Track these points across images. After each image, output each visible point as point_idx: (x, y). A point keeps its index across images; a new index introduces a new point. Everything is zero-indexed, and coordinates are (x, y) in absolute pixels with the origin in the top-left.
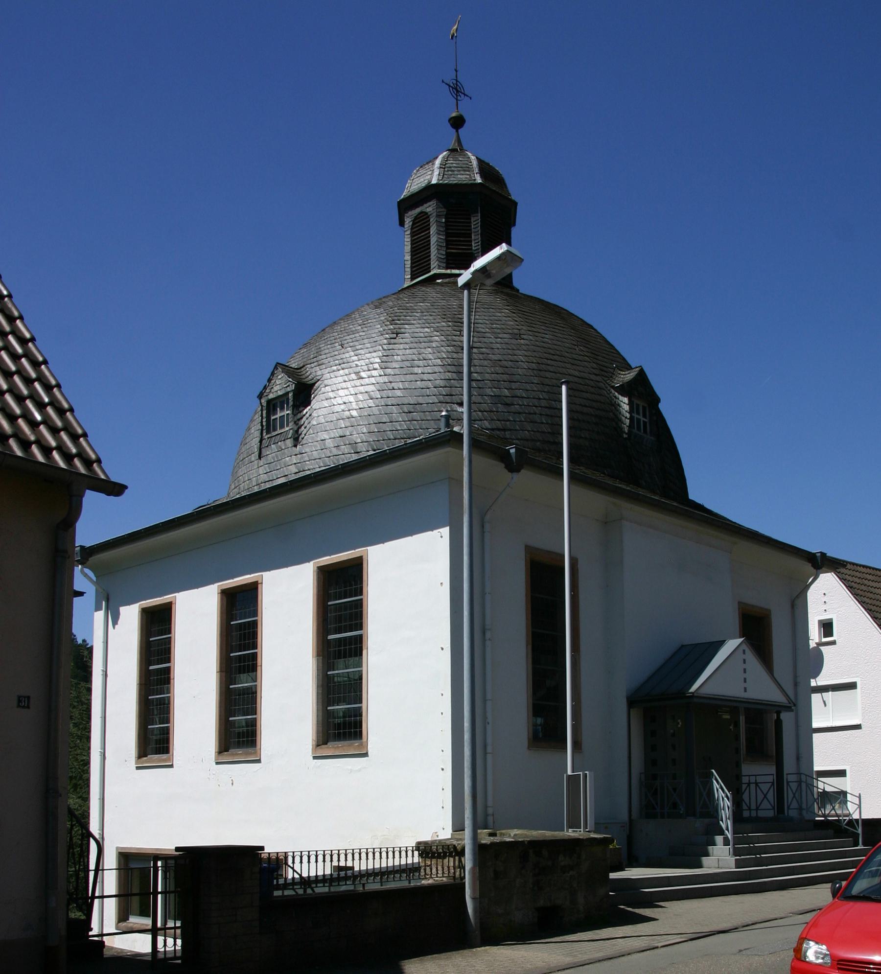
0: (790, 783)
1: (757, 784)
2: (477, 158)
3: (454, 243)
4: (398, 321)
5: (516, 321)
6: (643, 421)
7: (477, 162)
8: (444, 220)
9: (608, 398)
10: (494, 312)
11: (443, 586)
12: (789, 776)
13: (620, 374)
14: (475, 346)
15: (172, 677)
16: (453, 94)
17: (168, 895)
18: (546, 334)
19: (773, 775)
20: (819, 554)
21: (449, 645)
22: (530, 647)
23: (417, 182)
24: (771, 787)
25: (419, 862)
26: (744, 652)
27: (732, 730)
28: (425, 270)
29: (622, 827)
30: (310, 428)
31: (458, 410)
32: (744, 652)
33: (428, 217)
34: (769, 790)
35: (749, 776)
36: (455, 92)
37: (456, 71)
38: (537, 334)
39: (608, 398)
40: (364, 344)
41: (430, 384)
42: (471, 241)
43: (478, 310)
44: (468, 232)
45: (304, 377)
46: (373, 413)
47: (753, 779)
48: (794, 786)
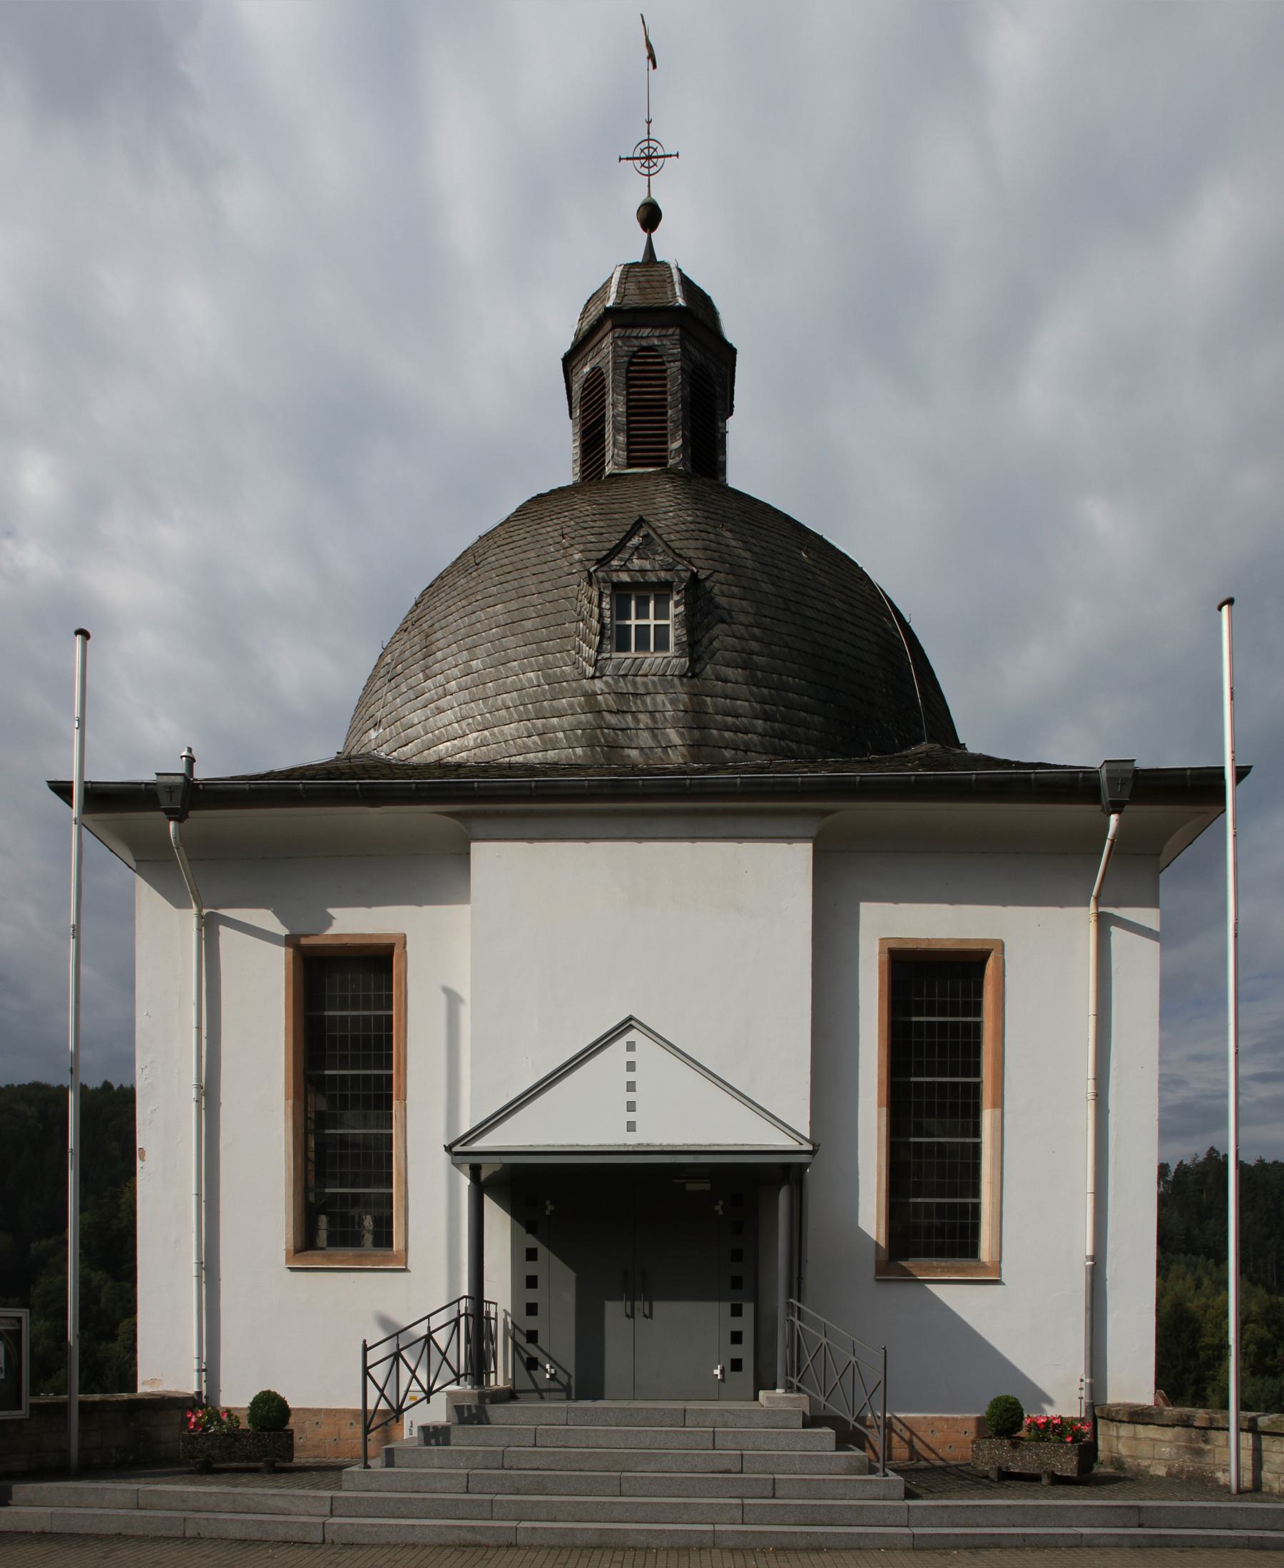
32: (631, 1046)
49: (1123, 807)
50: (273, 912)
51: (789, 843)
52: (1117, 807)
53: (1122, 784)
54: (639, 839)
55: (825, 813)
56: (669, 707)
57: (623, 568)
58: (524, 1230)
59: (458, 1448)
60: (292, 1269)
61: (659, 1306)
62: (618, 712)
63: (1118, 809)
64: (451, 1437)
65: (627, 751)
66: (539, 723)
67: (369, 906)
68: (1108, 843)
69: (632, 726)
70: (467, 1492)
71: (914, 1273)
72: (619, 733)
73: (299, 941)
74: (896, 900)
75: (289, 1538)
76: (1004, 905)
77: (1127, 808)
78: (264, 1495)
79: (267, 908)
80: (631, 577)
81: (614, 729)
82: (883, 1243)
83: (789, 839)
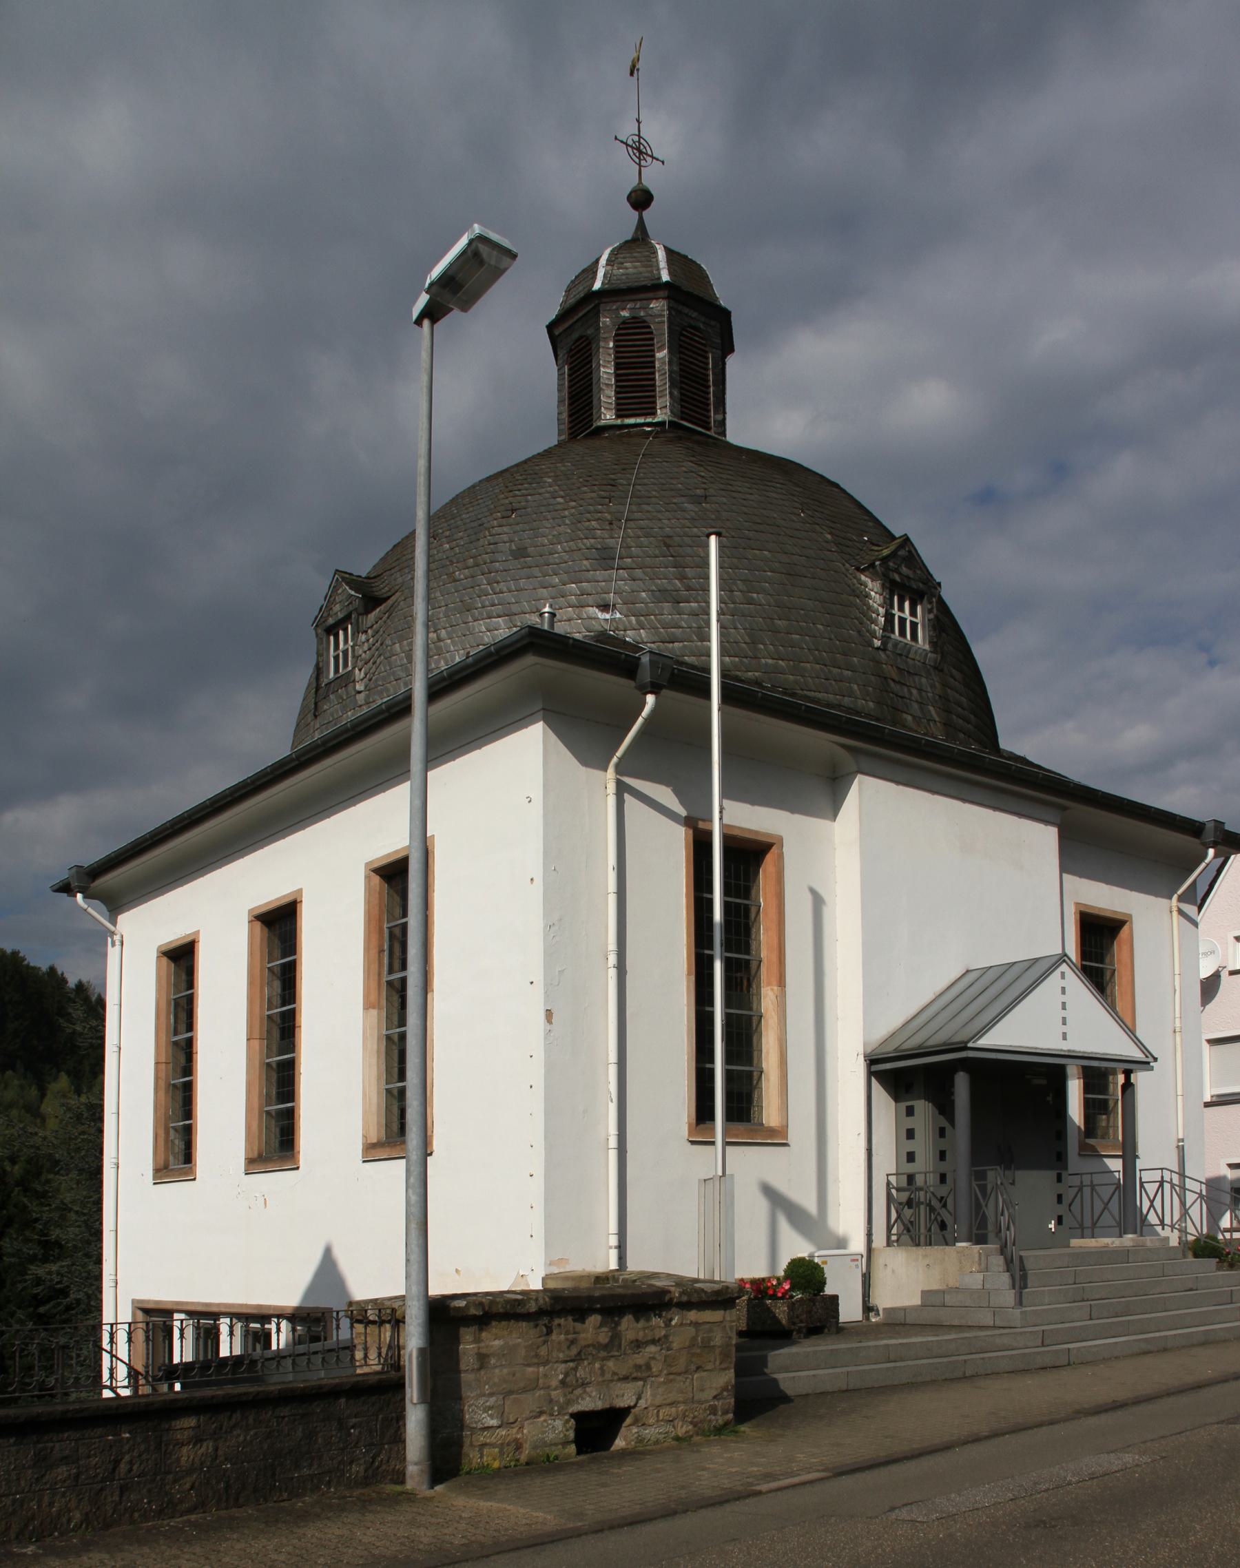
0: (1145, 1184)
1: (1093, 1187)
2: (665, 247)
3: (646, 389)
4: (517, 492)
5: (703, 477)
6: (899, 617)
7: (664, 253)
8: (611, 345)
9: (849, 586)
10: (668, 467)
11: (534, 882)
12: (1142, 1172)
13: (873, 550)
14: (633, 517)
15: (194, 1052)
16: (634, 157)
17: (210, 1357)
18: (751, 494)
19: (1119, 1171)
20: (1212, 824)
21: (542, 978)
22: (693, 978)
23: (574, 293)
24: (1077, 1193)
25: (352, 1338)
26: (1063, 975)
27: (1051, 1102)
28: (586, 424)
29: (853, 1260)
30: (380, 663)
31: (600, 617)
32: (1063, 975)
33: (590, 343)
34: (1111, 1198)
35: (1091, 1174)
36: (637, 154)
37: (638, 121)
38: (734, 494)
39: (849, 586)
40: (496, 543)
41: (557, 580)
42: (654, 373)
43: (644, 465)
44: (649, 359)
45: (378, 588)
46: (469, 631)
47: (1087, 1180)
48: (1151, 1189)
49: (661, 689)
50: (673, 790)
51: (1046, 825)
52: (655, 689)
53: (662, 669)
54: (964, 800)
55: (1064, 808)
56: (929, 689)
57: (897, 571)
58: (937, 1112)
59: (1033, 1289)
60: (693, 1143)
61: (1020, 1174)
62: (899, 683)
63: (656, 690)
64: (1029, 1281)
65: (905, 716)
66: (835, 671)
67: (753, 803)
68: (640, 721)
69: (907, 696)
70: (1091, 1319)
71: (1099, 1149)
72: (900, 699)
73: (697, 824)
74: (1081, 876)
75: (1045, 1365)
76: (1131, 890)
77: (664, 692)
78: (992, 1336)
79: (667, 785)
80: (901, 579)
81: (897, 695)
82: (1082, 1127)
83: (1047, 822)
